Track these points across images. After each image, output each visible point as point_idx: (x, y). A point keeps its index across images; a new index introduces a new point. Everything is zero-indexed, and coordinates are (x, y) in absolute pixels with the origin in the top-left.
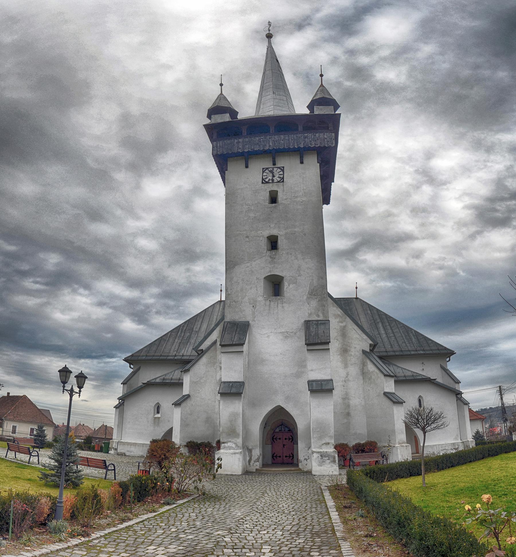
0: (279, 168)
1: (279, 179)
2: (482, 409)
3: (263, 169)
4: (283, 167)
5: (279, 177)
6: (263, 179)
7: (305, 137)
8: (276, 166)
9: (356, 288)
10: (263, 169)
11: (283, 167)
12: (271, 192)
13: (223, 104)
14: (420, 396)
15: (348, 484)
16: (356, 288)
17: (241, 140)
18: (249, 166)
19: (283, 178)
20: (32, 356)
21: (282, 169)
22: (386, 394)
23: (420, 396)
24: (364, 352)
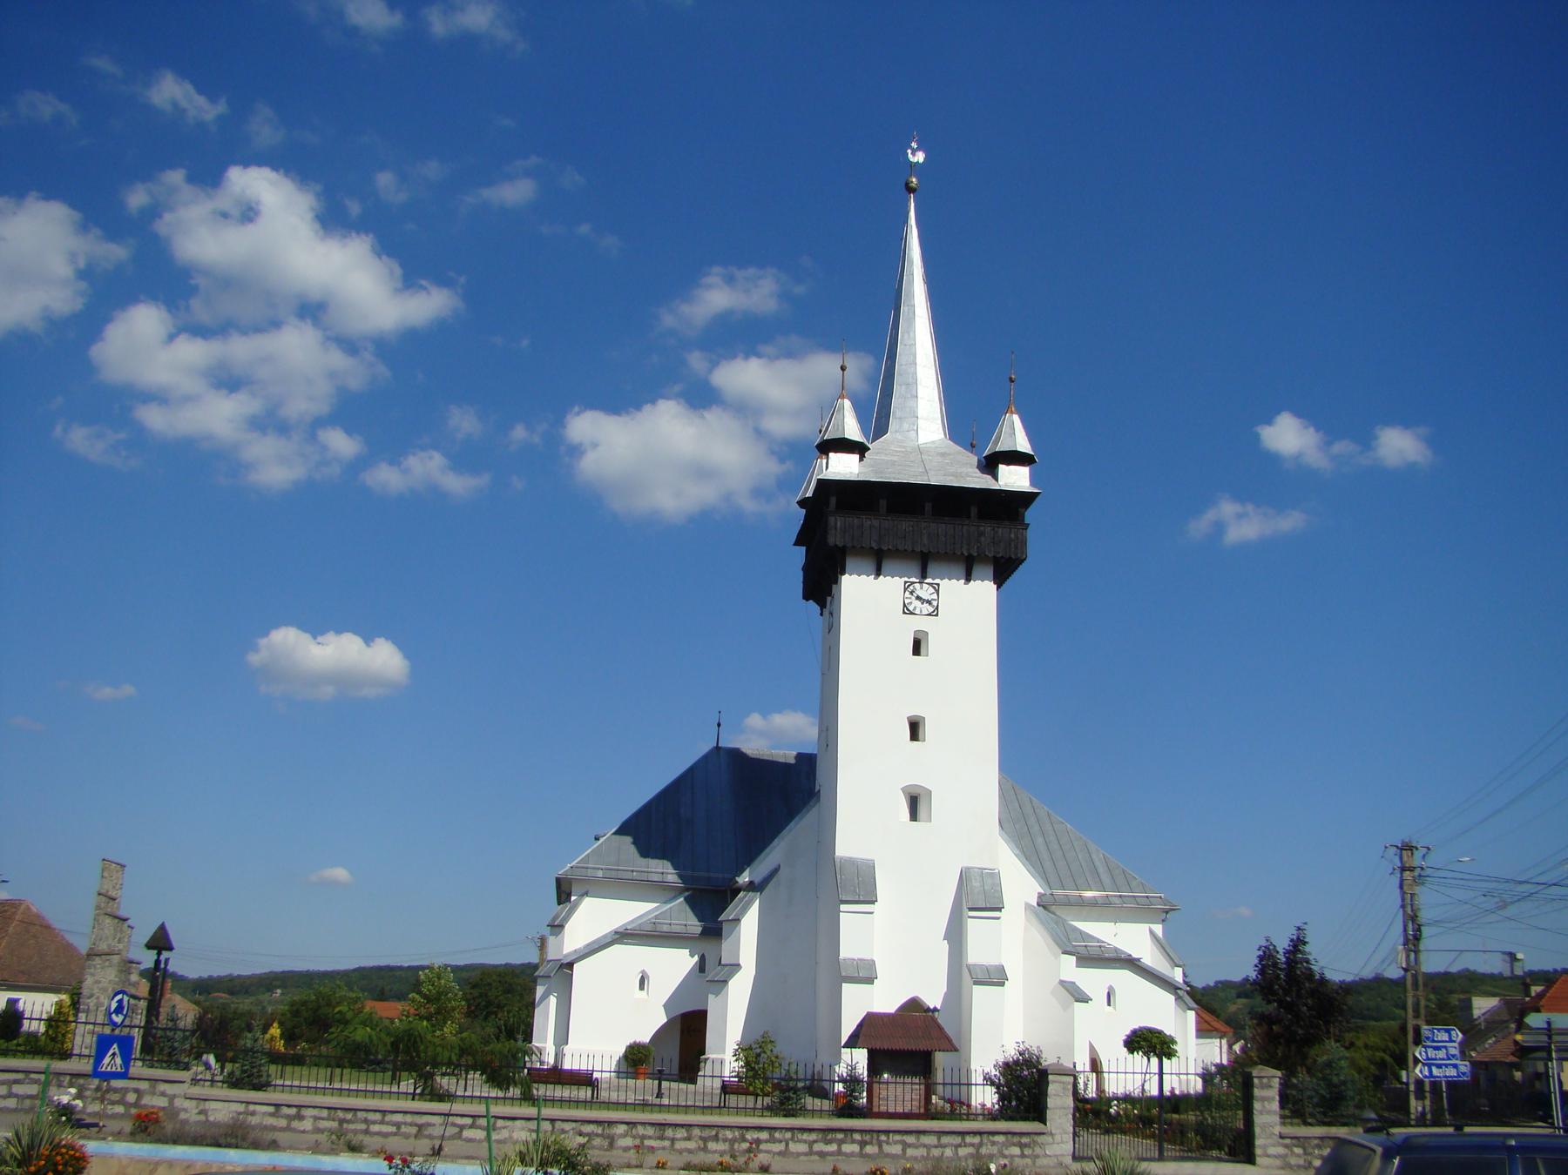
7: (981, 534)
17: (876, 523)
22: (1062, 983)
24: (1028, 906)
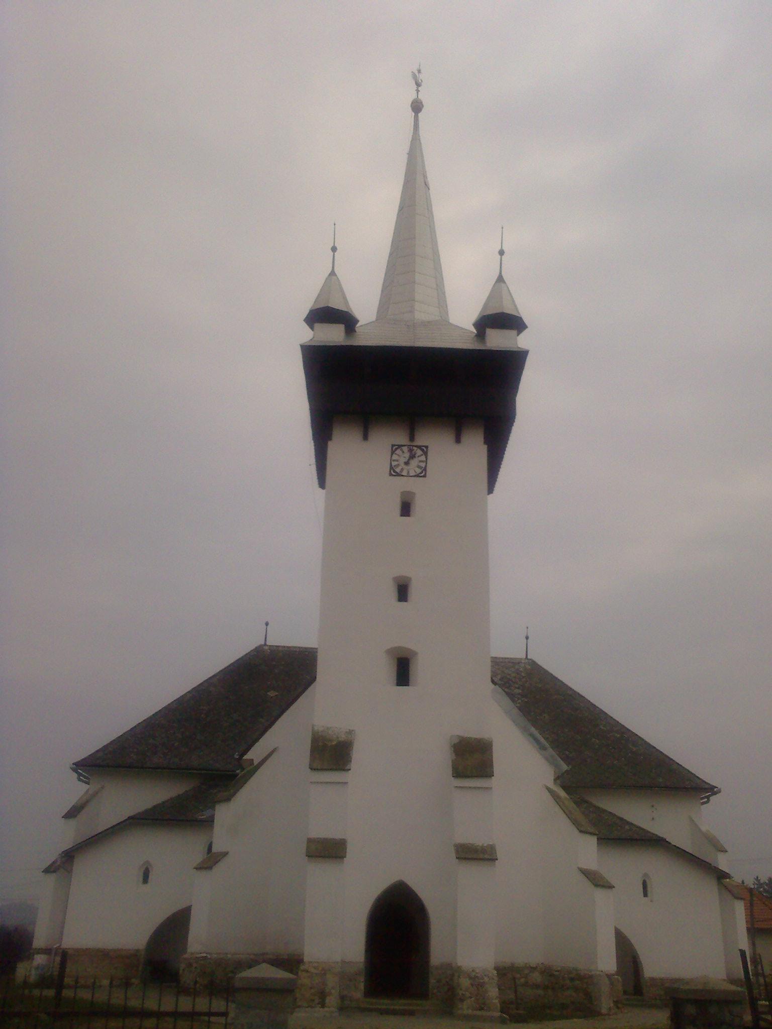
0: (419, 447)
1: (418, 471)
2: (513, 965)
3: (393, 446)
4: (427, 447)
5: (419, 467)
6: (391, 468)
8: (415, 443)
9: (501, 253)
10: (393, 446)
11: (427, 447)
12: (404, 494)
13: (336, 304)
14: (646, 875)
15: (568, 765)
16: (501, 253)
18: (370, 438)
19: (425, 469)
20: (432, 981)
21: (425, 450)
22: (586, 873)
23: (646, 875)
